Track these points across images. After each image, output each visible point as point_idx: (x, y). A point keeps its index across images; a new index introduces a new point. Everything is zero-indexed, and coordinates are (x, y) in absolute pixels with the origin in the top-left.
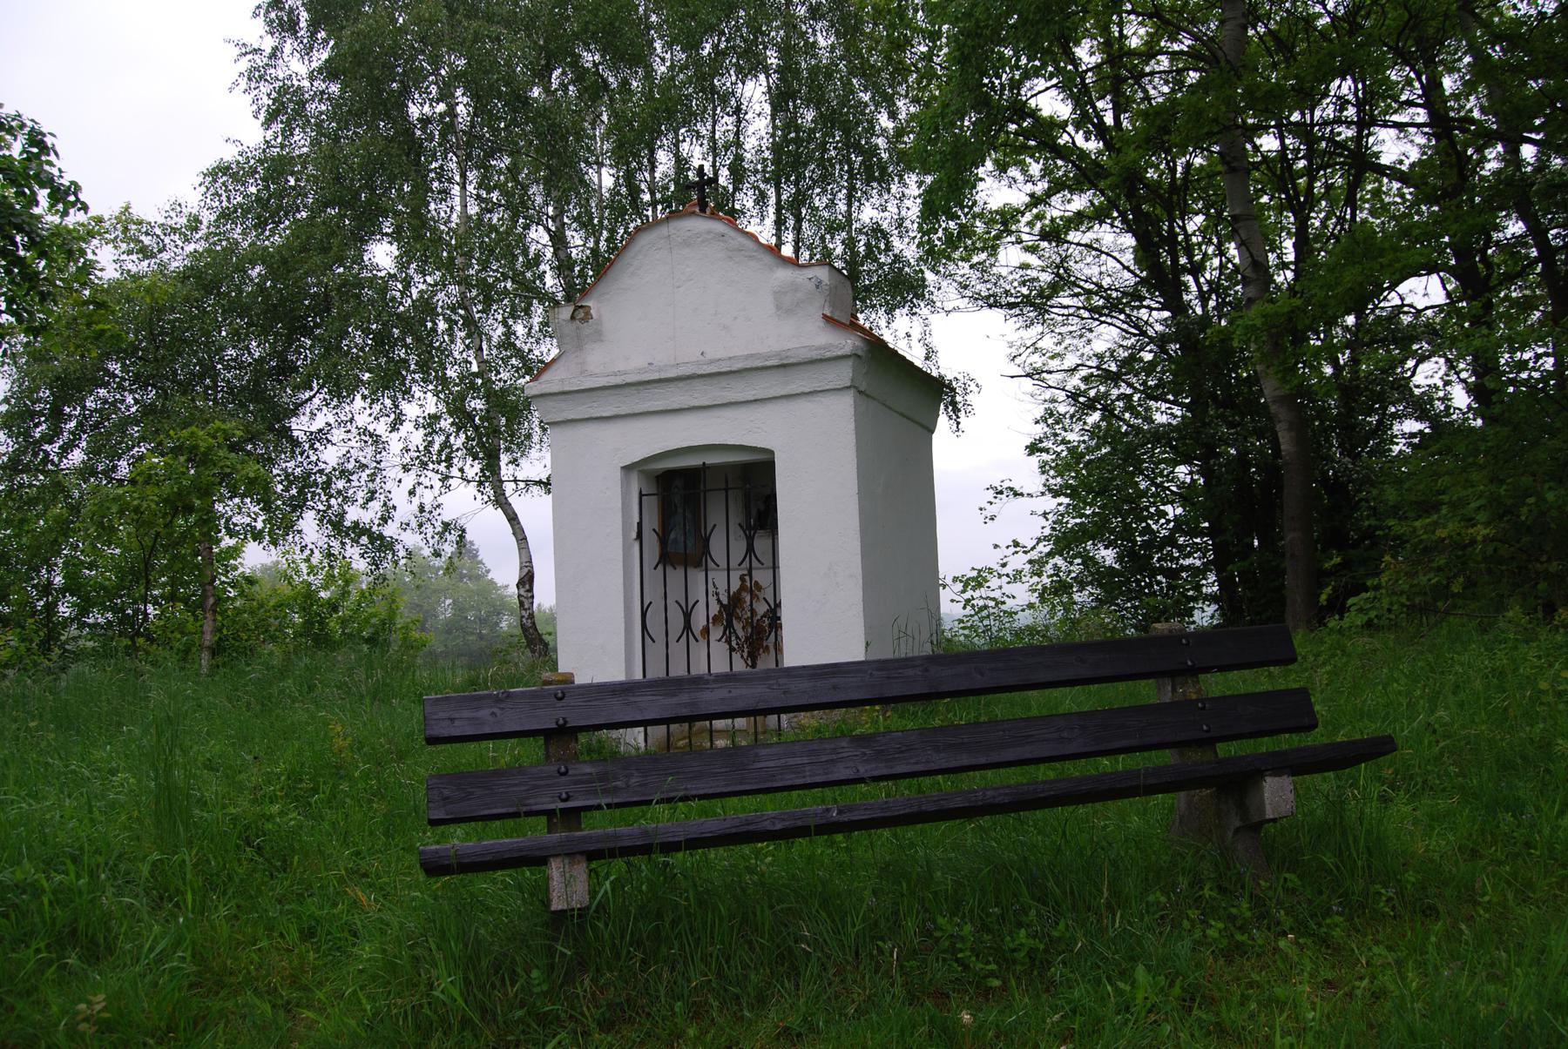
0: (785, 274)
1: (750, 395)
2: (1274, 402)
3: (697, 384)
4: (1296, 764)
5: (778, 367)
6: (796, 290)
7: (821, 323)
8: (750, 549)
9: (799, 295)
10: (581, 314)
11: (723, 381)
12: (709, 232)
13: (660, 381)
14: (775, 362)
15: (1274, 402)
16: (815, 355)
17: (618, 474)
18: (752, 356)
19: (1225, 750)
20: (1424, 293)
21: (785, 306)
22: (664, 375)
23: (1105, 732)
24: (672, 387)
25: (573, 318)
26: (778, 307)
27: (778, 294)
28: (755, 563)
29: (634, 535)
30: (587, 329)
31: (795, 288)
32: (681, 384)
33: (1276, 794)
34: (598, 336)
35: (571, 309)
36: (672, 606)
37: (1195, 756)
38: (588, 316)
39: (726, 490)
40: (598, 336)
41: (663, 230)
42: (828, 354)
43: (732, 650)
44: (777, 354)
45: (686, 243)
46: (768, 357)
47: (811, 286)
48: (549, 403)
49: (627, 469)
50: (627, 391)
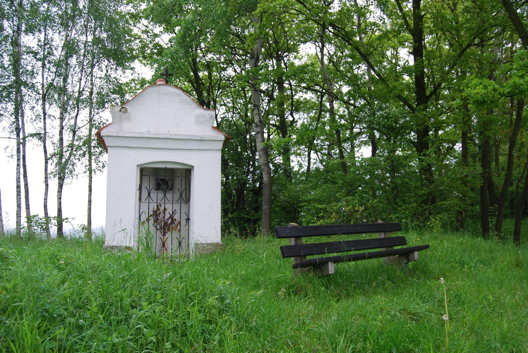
1: (187, 147)
3: (169, 141)
4: (336, 260)
7: (211, 128)
8: (149, 195)
10: (123, 110)
12: (174, 92)
13: (157, 138)
14: (199, 139)
16: (212, 138)
17: (136, 167)
19: (308, 258)
21: (199, 121)
22: (158, 137)
23: (378, 243)
25: (120, 111)
26: (197, 121)
28: (151, 200)
29: (138, 188)
30: (125, 115)
33: (331, 268)
34: (129, 119)
36: (183, 213)
37: (389, 249)
38: (126, 111)
40: (129, 119)
42: (216, 139)
43: (157, 229)
44: (200, 136)
47: (209, 116)
50: (143, 139)
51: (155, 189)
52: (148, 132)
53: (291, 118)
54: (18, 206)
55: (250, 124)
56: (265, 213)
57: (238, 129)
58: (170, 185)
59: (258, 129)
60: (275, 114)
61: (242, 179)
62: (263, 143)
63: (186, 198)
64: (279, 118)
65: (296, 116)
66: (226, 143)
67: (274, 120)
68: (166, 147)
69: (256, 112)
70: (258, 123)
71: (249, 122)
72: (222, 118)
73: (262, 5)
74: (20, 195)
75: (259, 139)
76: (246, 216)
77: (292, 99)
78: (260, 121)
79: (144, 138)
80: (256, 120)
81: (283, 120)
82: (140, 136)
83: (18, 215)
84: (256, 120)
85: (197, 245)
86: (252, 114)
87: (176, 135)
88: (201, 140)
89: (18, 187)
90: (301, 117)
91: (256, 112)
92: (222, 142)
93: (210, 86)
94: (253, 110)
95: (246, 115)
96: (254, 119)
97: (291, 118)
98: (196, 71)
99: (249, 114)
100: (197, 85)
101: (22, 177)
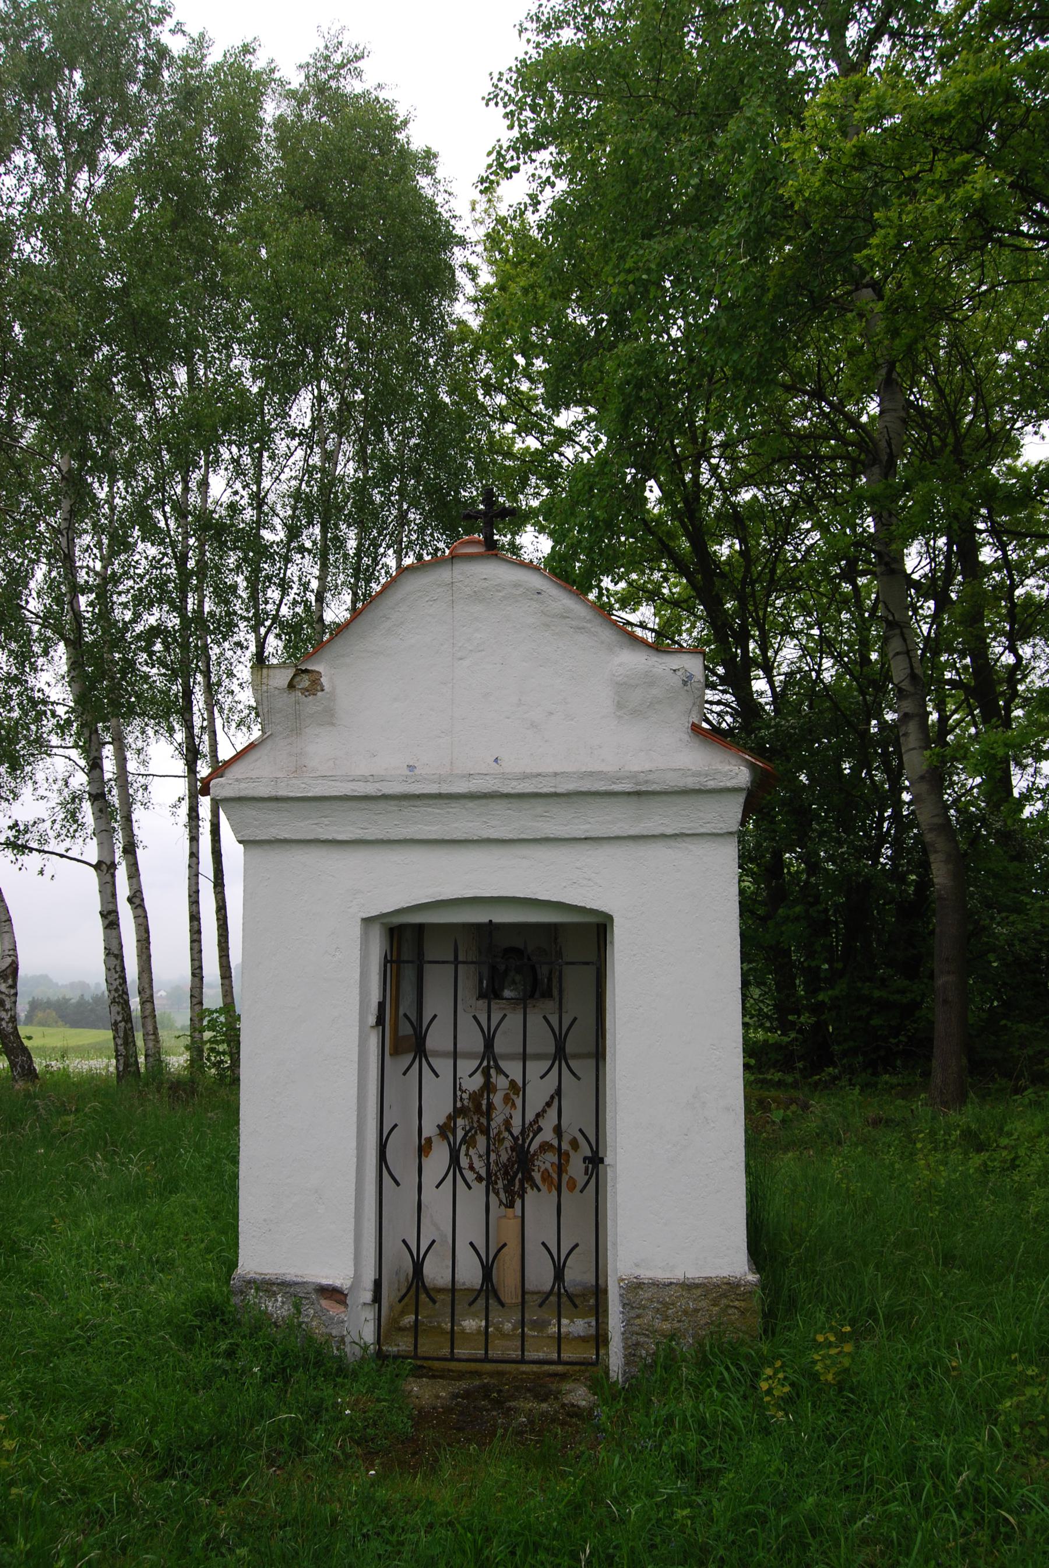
0: (634, 661)
2: (931, 830)
3: (498, 807)
5: (629, 794)
6: (651, 684)
7: (684, 734)
9: (655, 691)
10: (305, 682)
11: (539, 807)
12: (516, 585)
13: (439, 796)
15: (931, 830)
16: (690, 782)
17: (357, 930)
18: (591, 774)
20: (653, 337)
21: (630, 703)
22: (445, 789)
24: (455, 808)
25: (291, 686)
26: (619, 706)
27: (622, 687)
29: (372, 1020)
30: (311, 705)
31: (649, 680)
32: (470, 804)
34: (329, 717)
35: (290, 673)
38: (315, 686)
39: (456, 962)
41: (445, 574)
42: (712, 784)
44: (633, 776)
45: (477, 597)
46: (618, 779)
47: (676, 681)
48: (249, 812)
49: (367, 921)
50: (382, 805)
51: (481, 996)
52: (411, 768)
53: (1009, 659)
54: (193, 974)
55: (881, 689)
56: (945, 1002)
57: (836, 707)
58: (543, 971)
59: (908, 706)
60: (955, 651)
61: (858, 874)
62: (927, 753)
63: (583, 1046)
64: (968, 660)
65: (1026, 651)
66: (756, 802)
67: (955, 667)
68: (486, 834)
69: (896, 645)
70: (905, 685)
71: (873, 683)
72: (790, 675)
73: (893, 214)
74: (200, 941)
75: (912, 739)
76: (877, 994)
77: (1010, 596)
78: (913, 677)
79: (385, 797)
80: (899, 671)
81: (983, 664)
82: (370, 789)
83: (195, 1001)
84: (899, 671)
85: (634, 1287)
86: (882, 653)
87: (525, 777)
88: (638, 794)
89: (195, 918)
90: (1038, 651)
91: (896, 645)
92: (741, 799)
93: (744, 578)
94: (885, 640)
95: (865, 660)
96: (889, 670)
97: (1009, 659)
98: (700, 539)
99: (874, 656)
100: (706, 581)
101: (206, 888)
